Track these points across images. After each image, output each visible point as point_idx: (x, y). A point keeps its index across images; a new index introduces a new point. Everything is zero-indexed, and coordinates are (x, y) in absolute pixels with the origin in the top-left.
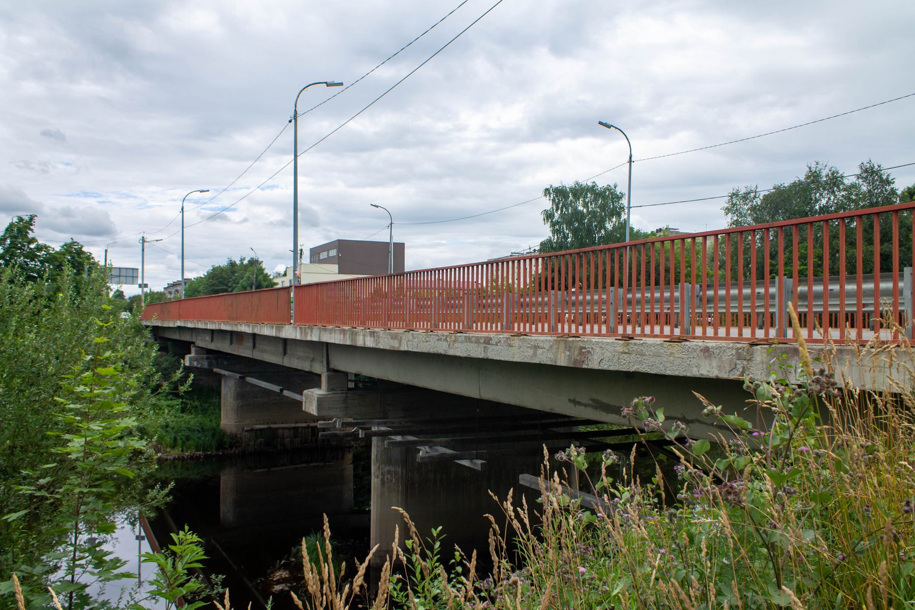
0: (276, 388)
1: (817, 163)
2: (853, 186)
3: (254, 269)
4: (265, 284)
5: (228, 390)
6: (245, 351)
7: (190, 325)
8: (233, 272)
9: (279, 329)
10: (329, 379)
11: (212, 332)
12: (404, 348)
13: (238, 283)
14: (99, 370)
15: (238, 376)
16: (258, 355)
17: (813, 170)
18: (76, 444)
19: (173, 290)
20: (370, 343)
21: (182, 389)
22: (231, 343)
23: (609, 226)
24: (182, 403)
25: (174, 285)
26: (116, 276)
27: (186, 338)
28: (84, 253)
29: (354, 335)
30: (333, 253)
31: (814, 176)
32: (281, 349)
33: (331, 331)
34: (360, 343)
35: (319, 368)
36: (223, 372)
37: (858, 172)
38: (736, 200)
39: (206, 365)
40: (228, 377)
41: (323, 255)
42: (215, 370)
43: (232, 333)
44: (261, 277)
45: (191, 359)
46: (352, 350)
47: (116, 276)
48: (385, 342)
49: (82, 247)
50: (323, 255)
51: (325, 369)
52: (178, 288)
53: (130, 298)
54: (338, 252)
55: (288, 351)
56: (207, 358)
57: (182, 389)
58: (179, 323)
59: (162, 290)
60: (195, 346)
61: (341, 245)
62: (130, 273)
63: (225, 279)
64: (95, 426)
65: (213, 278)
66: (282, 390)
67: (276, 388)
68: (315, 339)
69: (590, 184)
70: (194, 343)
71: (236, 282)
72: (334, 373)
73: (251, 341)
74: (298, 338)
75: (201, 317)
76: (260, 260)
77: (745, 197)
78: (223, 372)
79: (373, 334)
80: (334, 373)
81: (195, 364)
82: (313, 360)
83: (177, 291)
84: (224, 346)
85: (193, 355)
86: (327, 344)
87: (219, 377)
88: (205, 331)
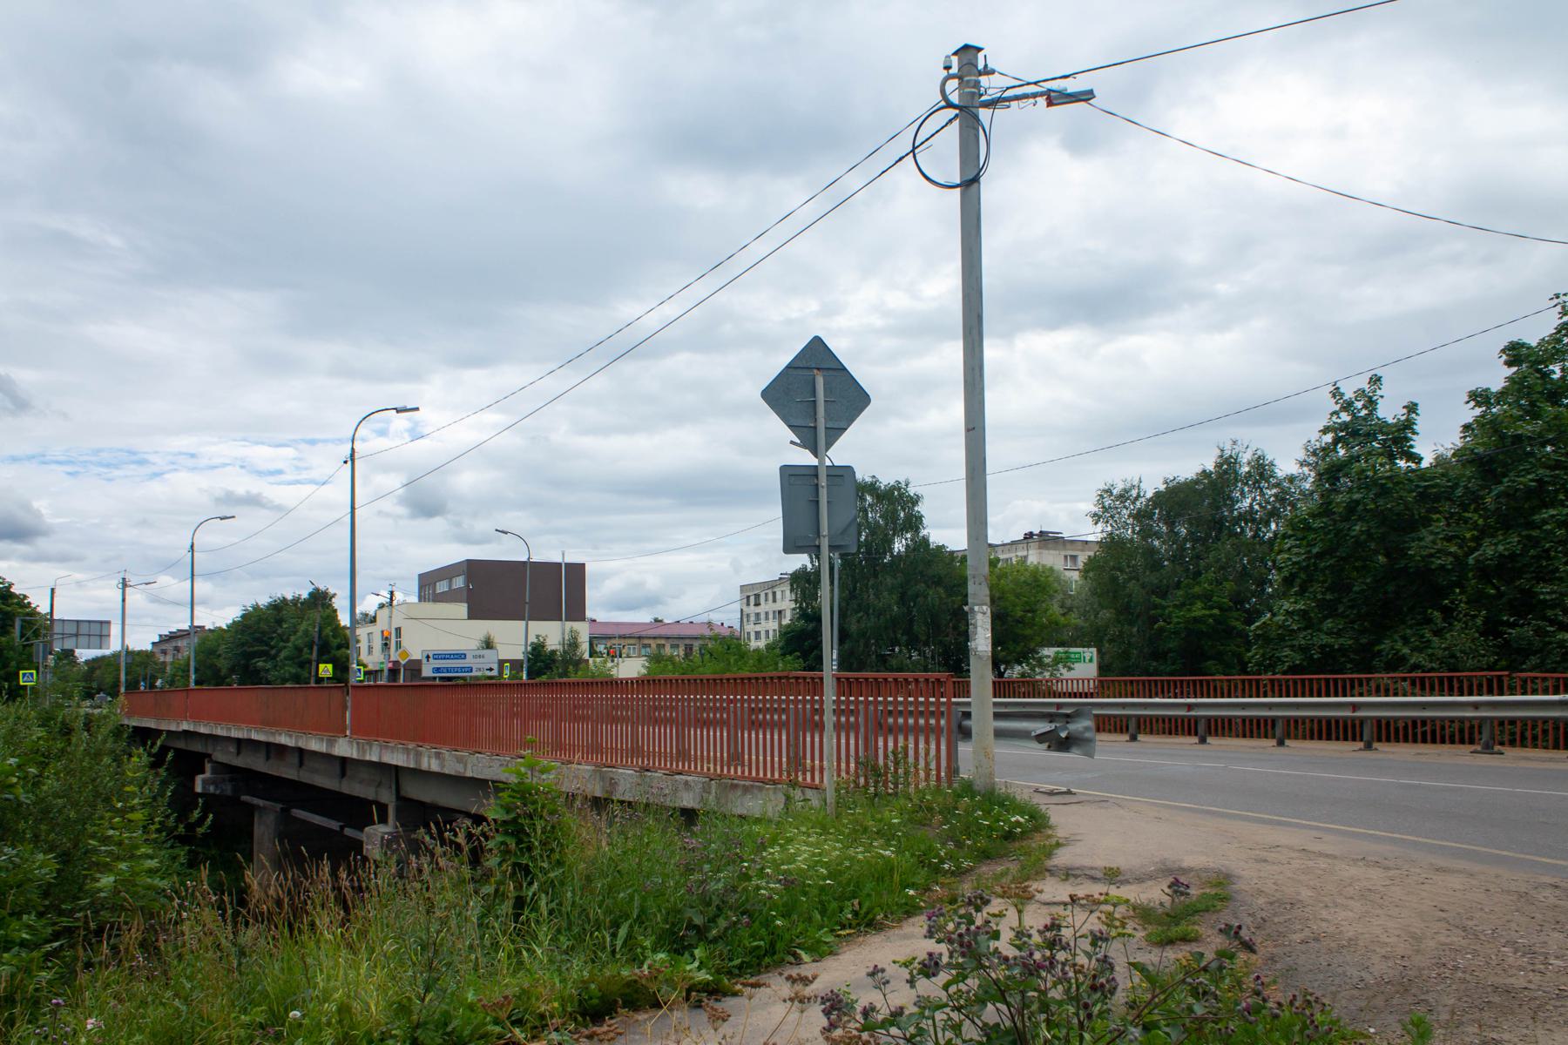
0: (334, 825)
1: (1235, 443)
2: (1291, 479)
3: (316, 615)
4: (335, 642)
5: (264, 830)
6: (288, 772)
7: (203, 730)
8: (279, 622)
9: (331, 743)
10: (398, 811)
11: (239, 741)
12: (469, 774)
13: (288, 640)
14: (129, 816)
15: (279, 806)
16: (305, 777)
17: (1227, 453)
18: (107, 880)
19: (169, 646)
20: (435, 766)
21: (200, 830)
22: (268, 758)
23: (899, 546)
24: (190, 851)
25: (173, 637)
26: (71, 635)
27: (198, 747)
28: (13, 595)
29: (418, 755)
30: (459, 582)
31: (1227, 465)
32: (337, 769)
33: (393, 750)
34: (424, 766)
35: (387, 797)
36: (256, 801)
37: (1302, 455)
38: (1112, 502)
39: (228, 789)
40: (265, 808)
41: (442, 587)
42: (245, 798)
43: (268, 744)
44: (328, 631)
45: (204, 782)
46: (417, 773)
47: (71, 635)
48: (451, 767)
49: (11, 585)
50: (442, 587)
51: (393, 798)
52: (179, 643)
53: (87, 662)
54: (468, 580)
55: (349, 773)
56: (231, 780)
57: (200, 830)
58: (185, 726)
59: (149, 648)
60: (211, 761)
61: (473, 569)
62: (95, 629)
63: (263, 633)
64: (123, 866)
65: (243, 632)
66: (342, 828)
67: (334, 825)
68: (375, 759)
69: (868, 480)
70: (209, 756)
71: (288, 644)
72: (405, 803)
73: (296, 760)
74: (355, 756)
75: (220, 718)
76: (332, 591)
77: (1123, 497)
78: (256, 801)
79: (438, 755)
80: (405, 803)
81: (212, 789)
82: (379, 785)
83: (177, 649)
84: (258, 764)
85: (208, 775)
86: (396, 767)
87: (251, 809)
88: (229, 739)
